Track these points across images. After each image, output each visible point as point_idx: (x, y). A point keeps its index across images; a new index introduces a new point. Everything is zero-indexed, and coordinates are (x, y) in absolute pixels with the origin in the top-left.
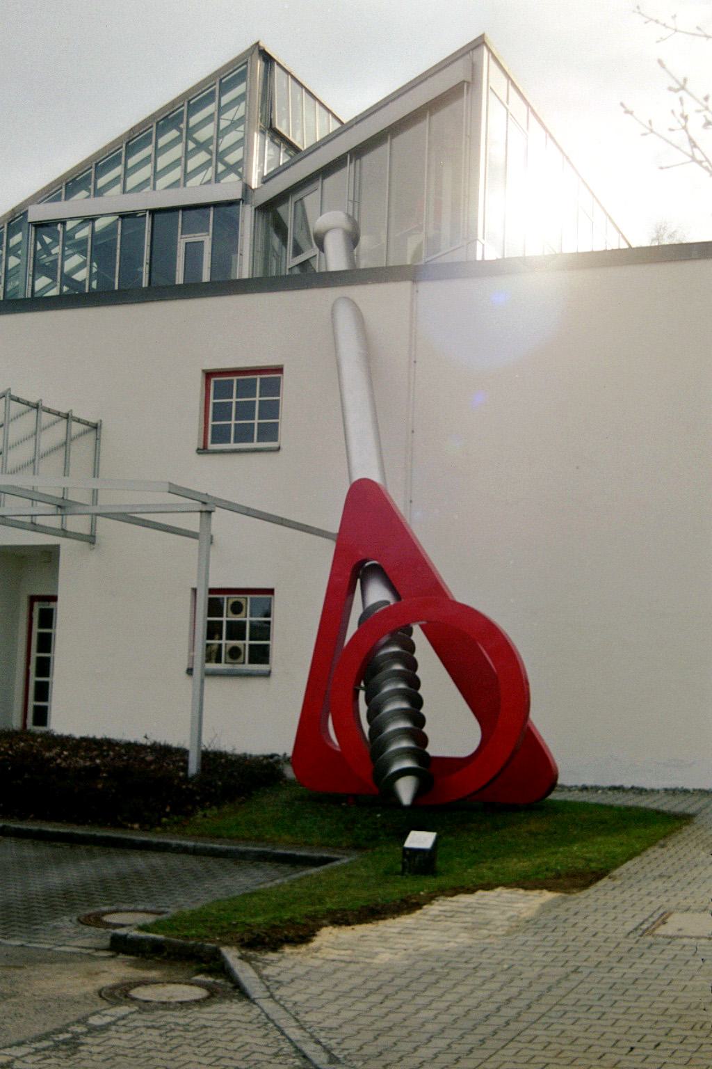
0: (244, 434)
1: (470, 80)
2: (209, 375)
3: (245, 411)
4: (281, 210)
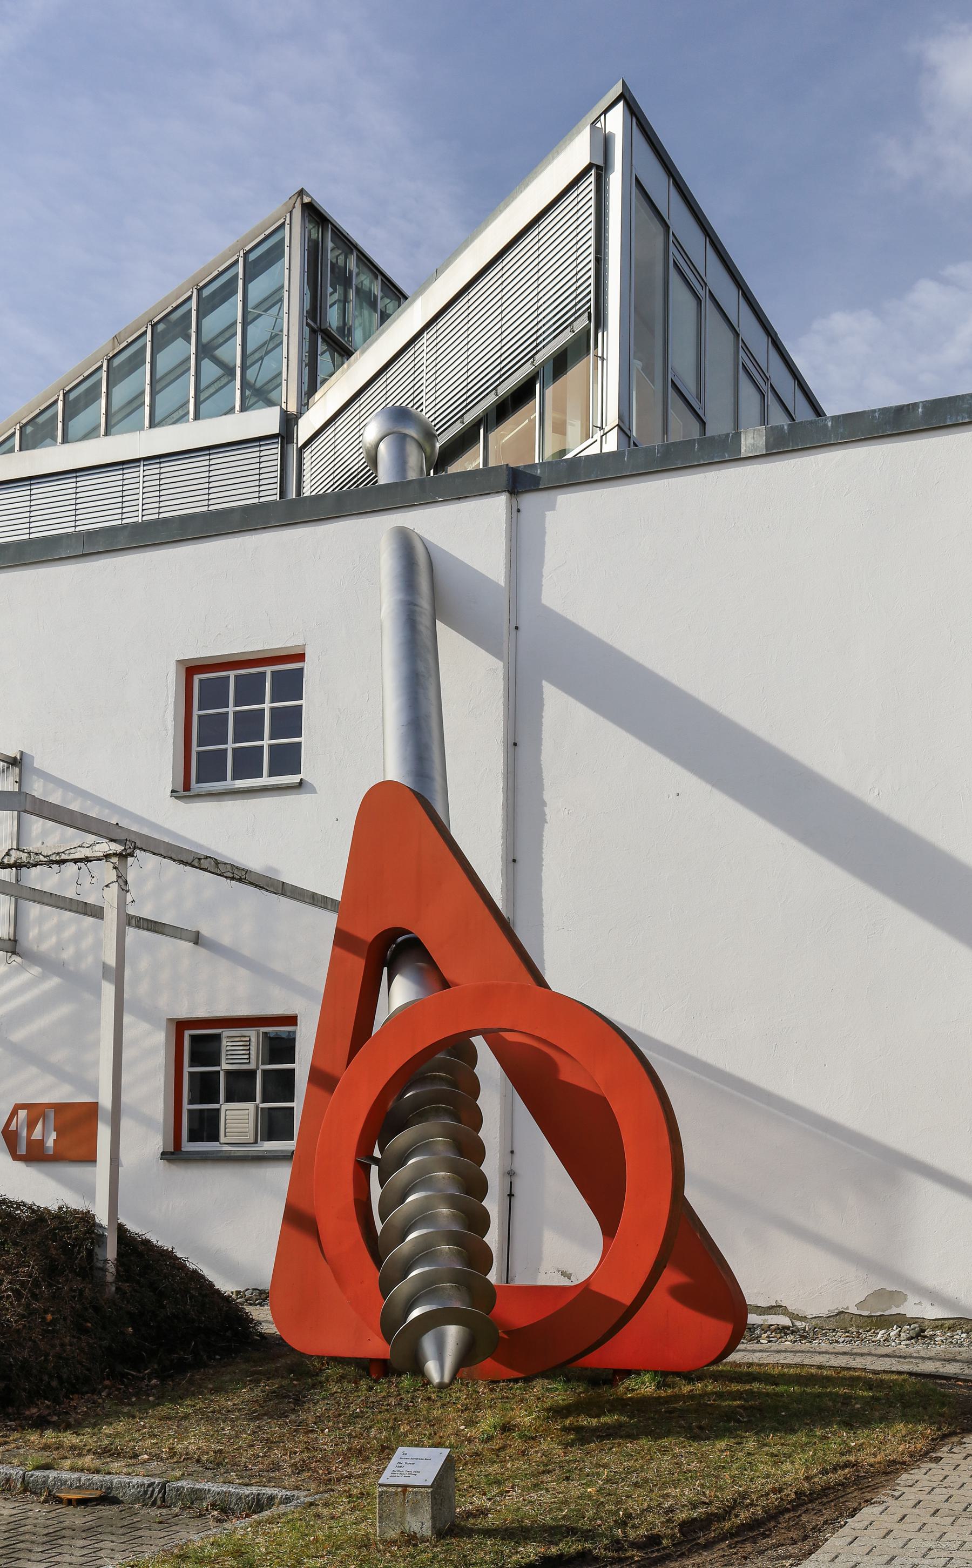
0: (248, 764)
1: (601, 163)
2: (191, 669)
3: (249, 725)
4: (271, 494)
